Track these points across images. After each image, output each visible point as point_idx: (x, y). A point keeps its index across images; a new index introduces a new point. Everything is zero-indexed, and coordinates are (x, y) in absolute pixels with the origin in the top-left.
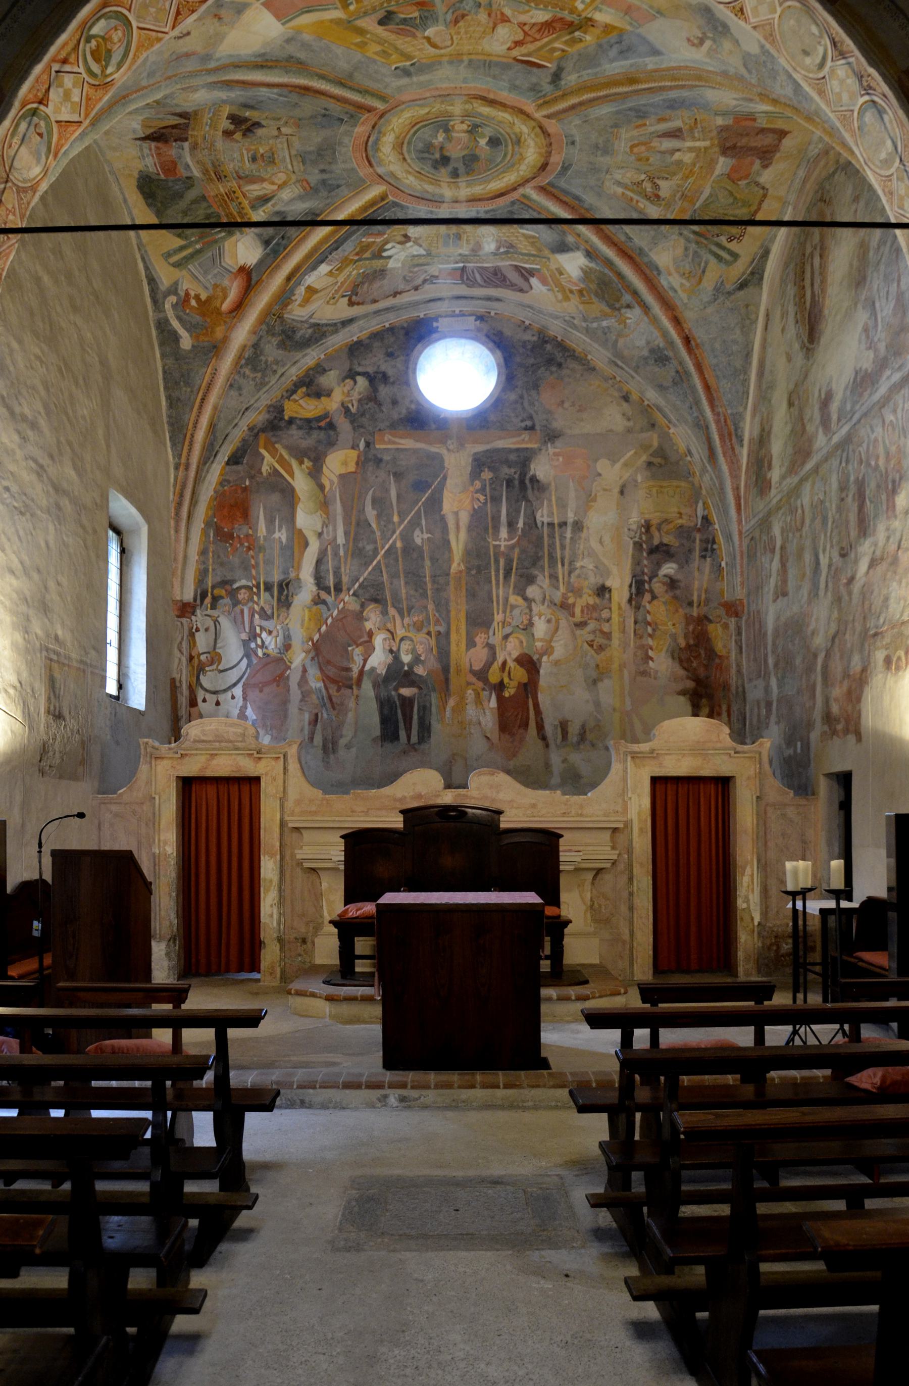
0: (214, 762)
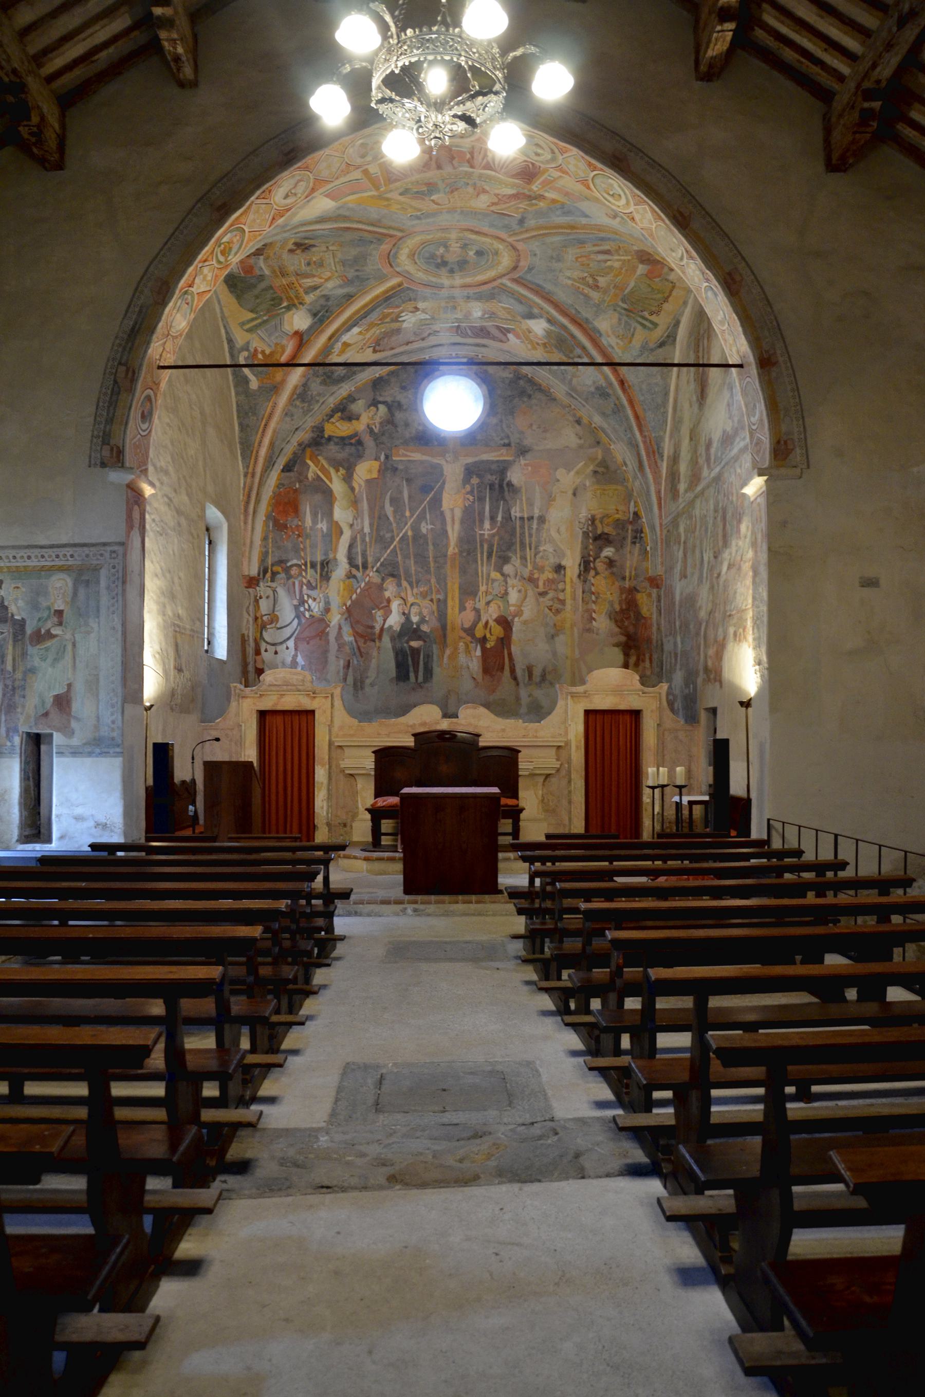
0: (283, 700)
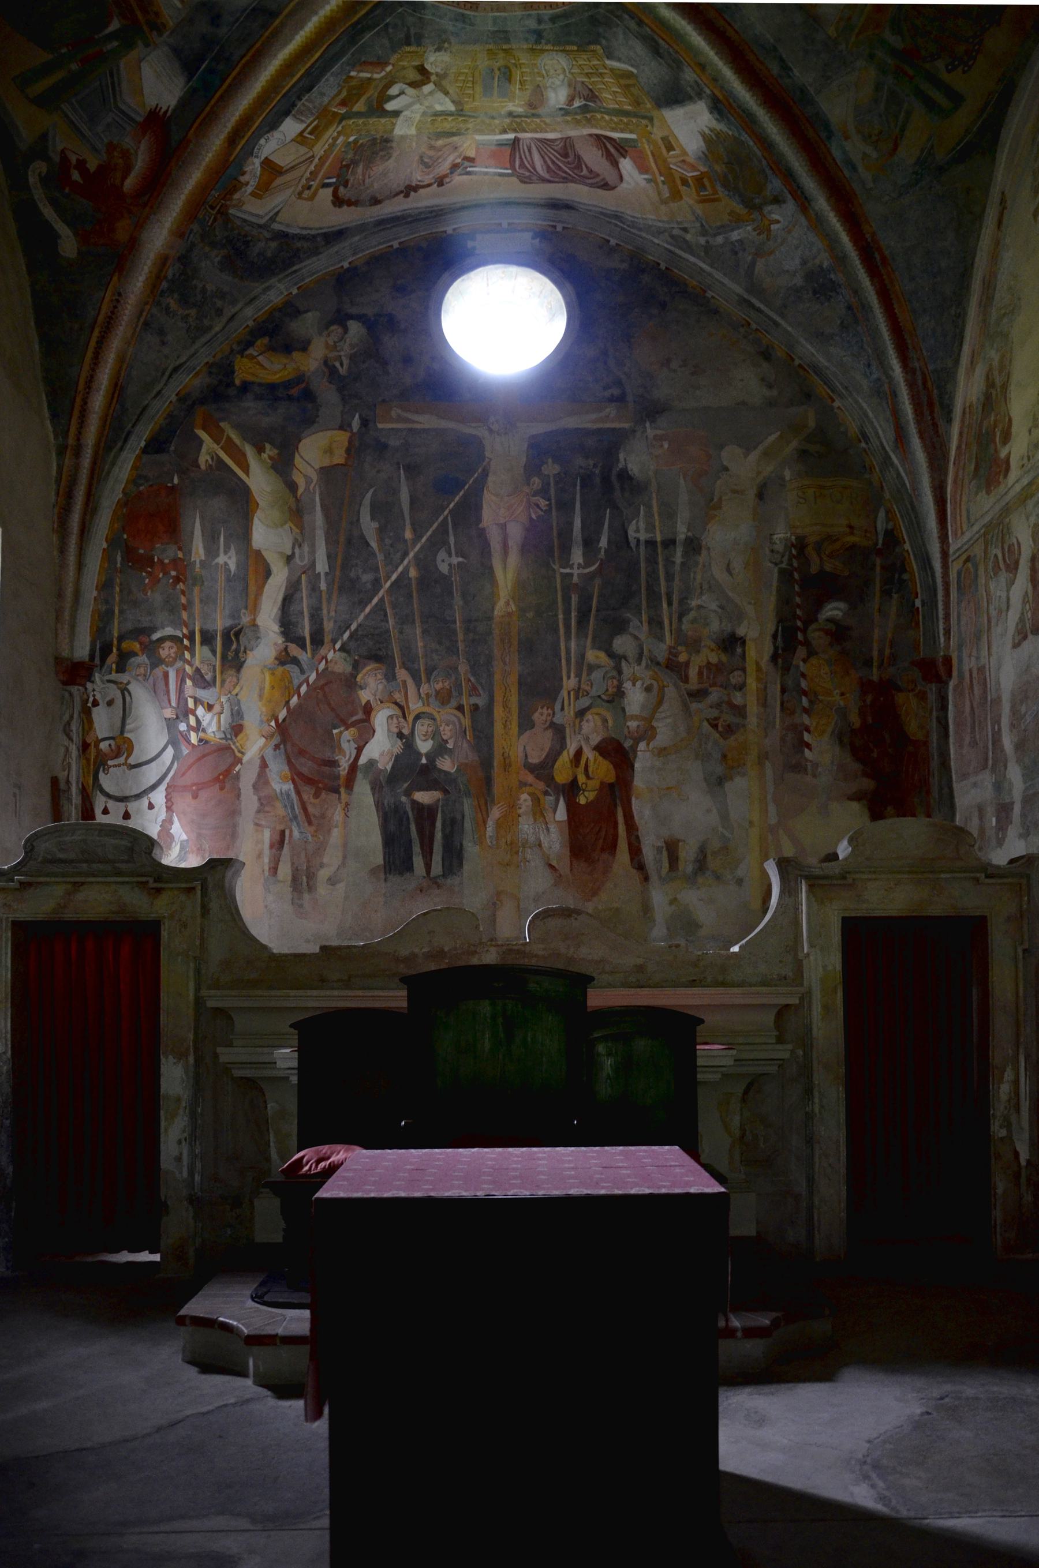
0: (80, 896)
